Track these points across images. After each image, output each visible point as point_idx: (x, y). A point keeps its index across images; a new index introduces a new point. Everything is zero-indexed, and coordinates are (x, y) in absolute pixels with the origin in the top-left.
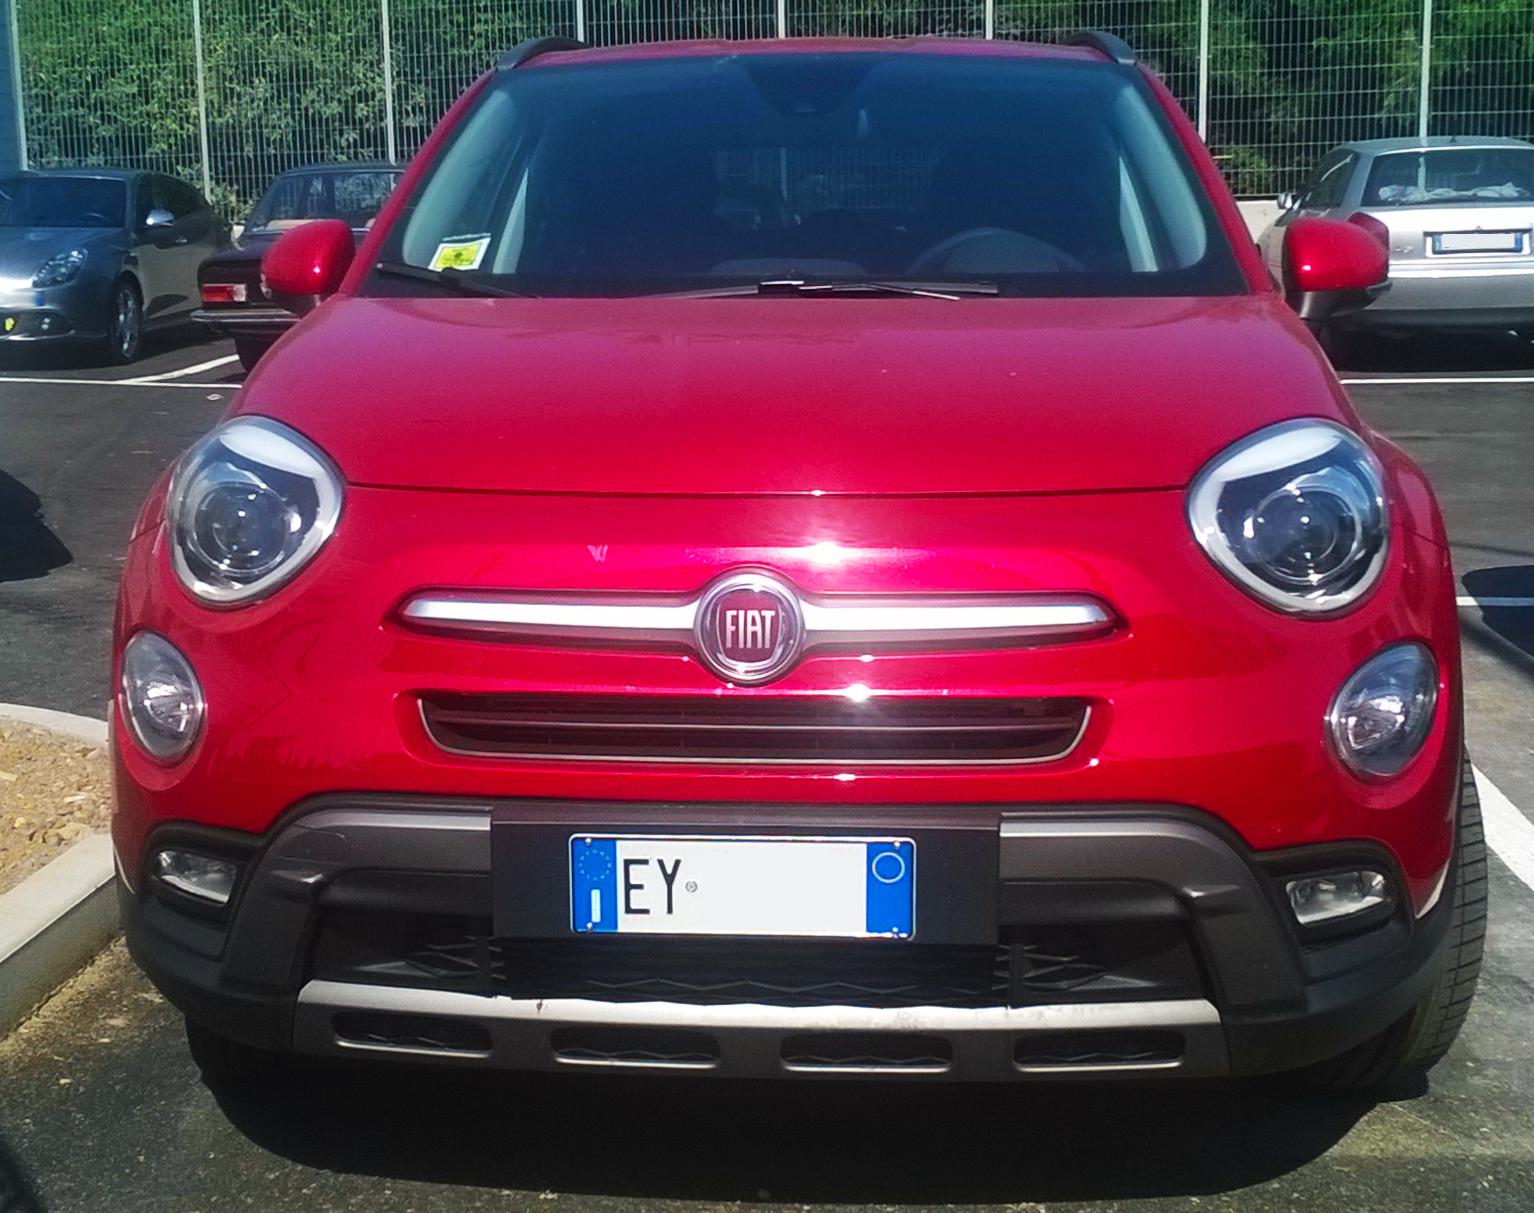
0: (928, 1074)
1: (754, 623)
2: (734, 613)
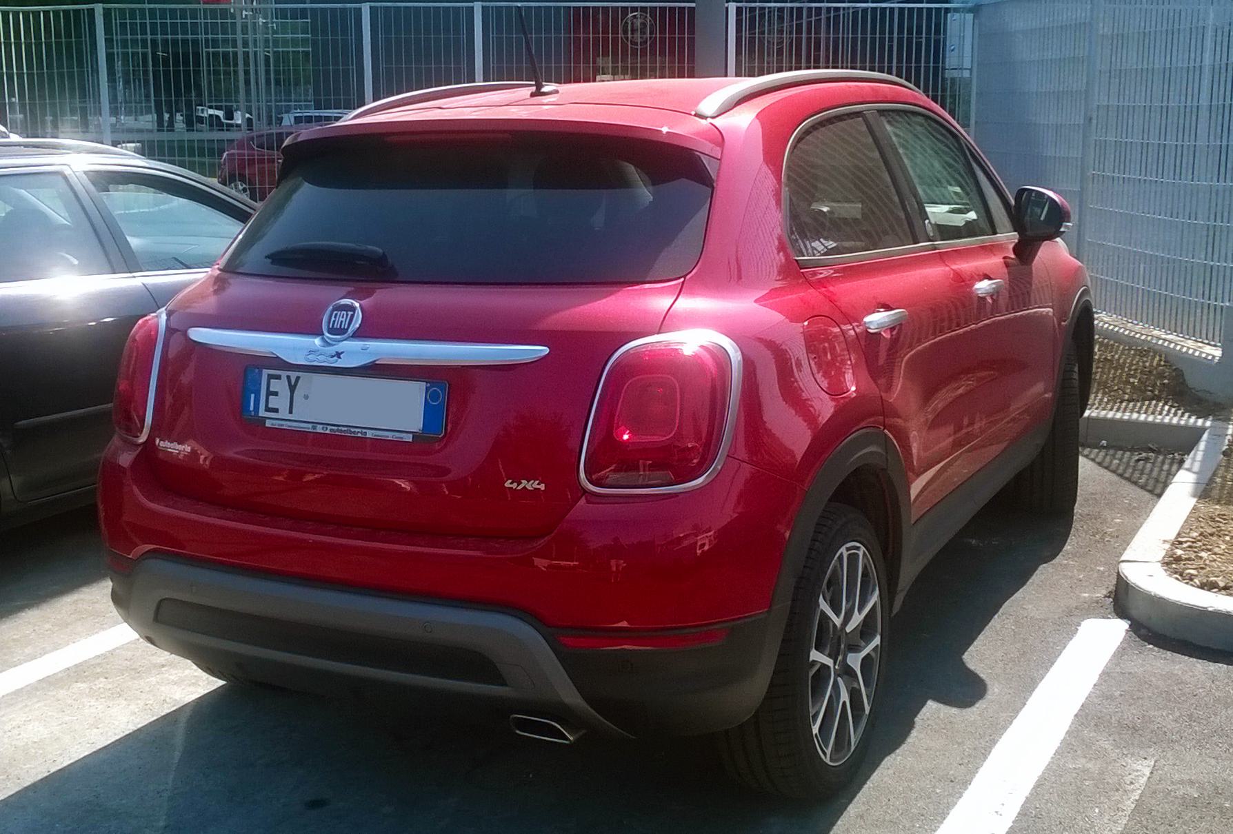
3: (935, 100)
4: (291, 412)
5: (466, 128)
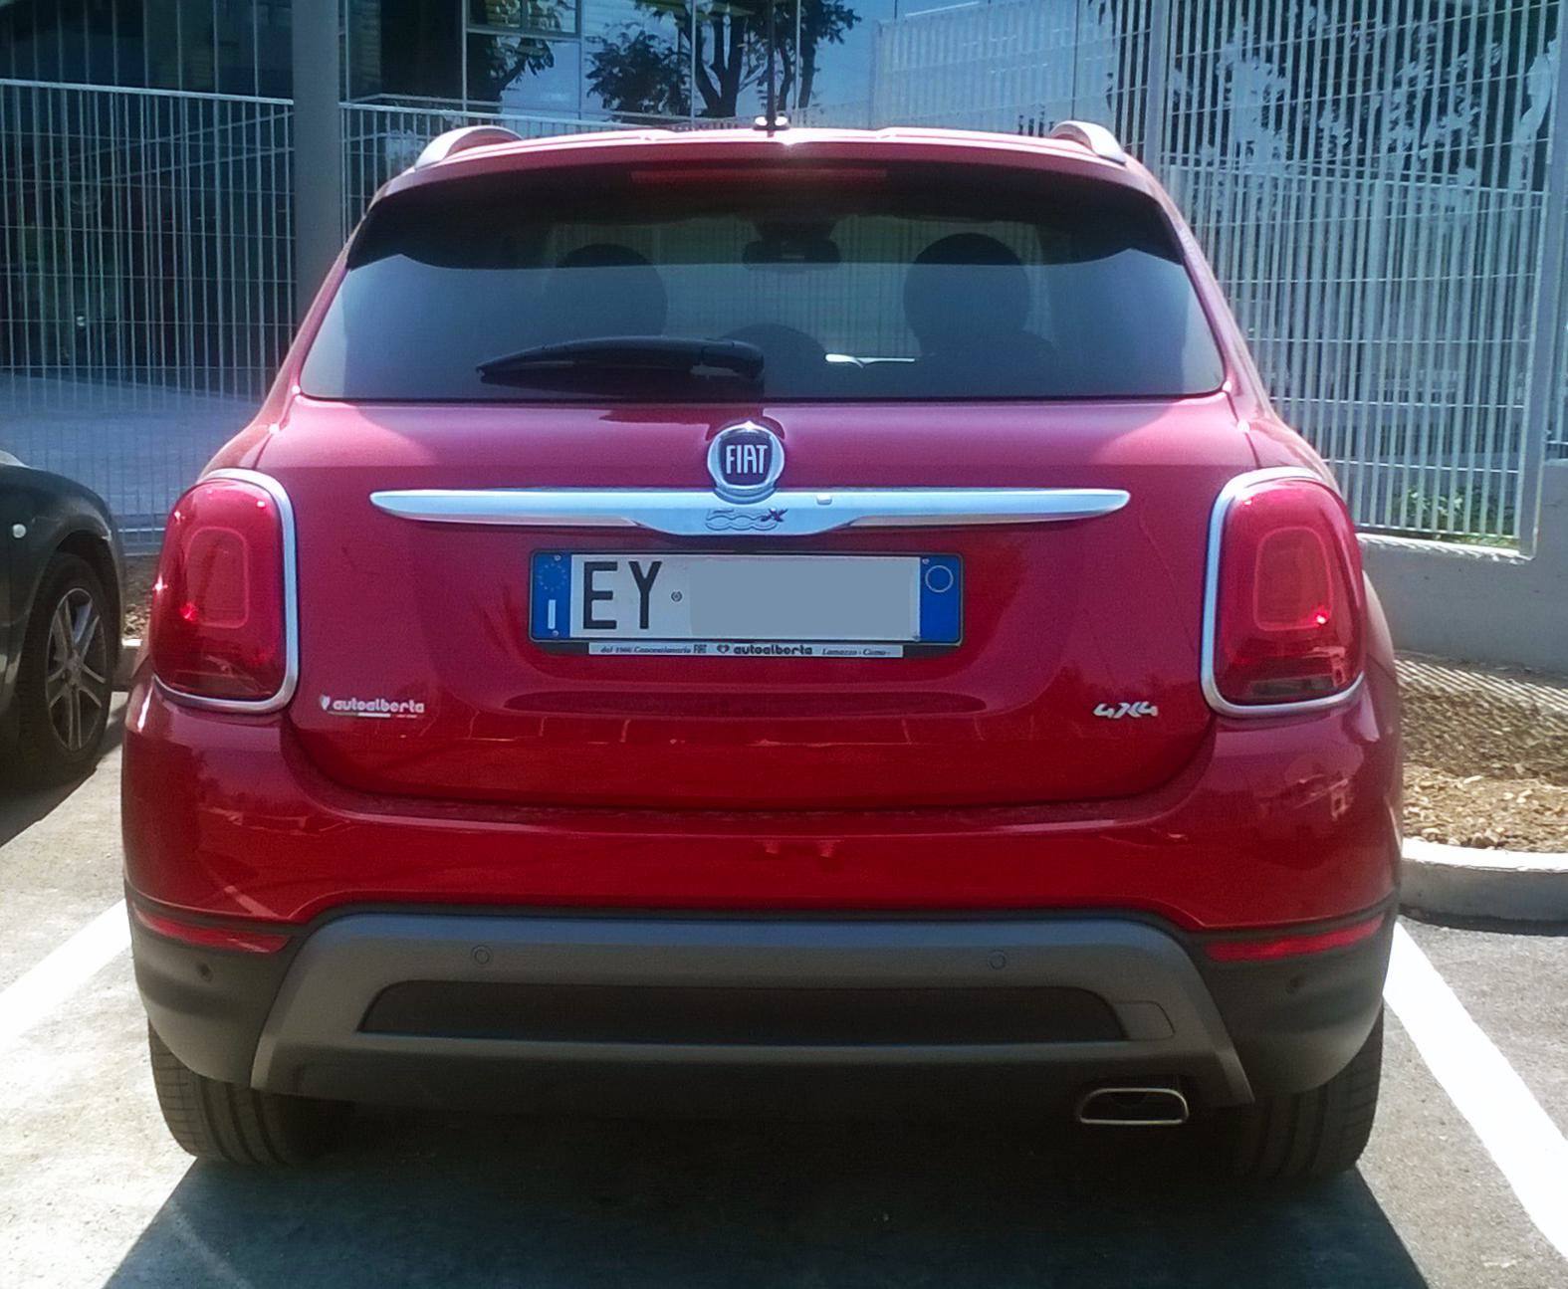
0: (461, 75)
1: (750, 454)
2: (733, 447)
3: (1128, 150)
4: (644, 624)
5: (697, 156)
